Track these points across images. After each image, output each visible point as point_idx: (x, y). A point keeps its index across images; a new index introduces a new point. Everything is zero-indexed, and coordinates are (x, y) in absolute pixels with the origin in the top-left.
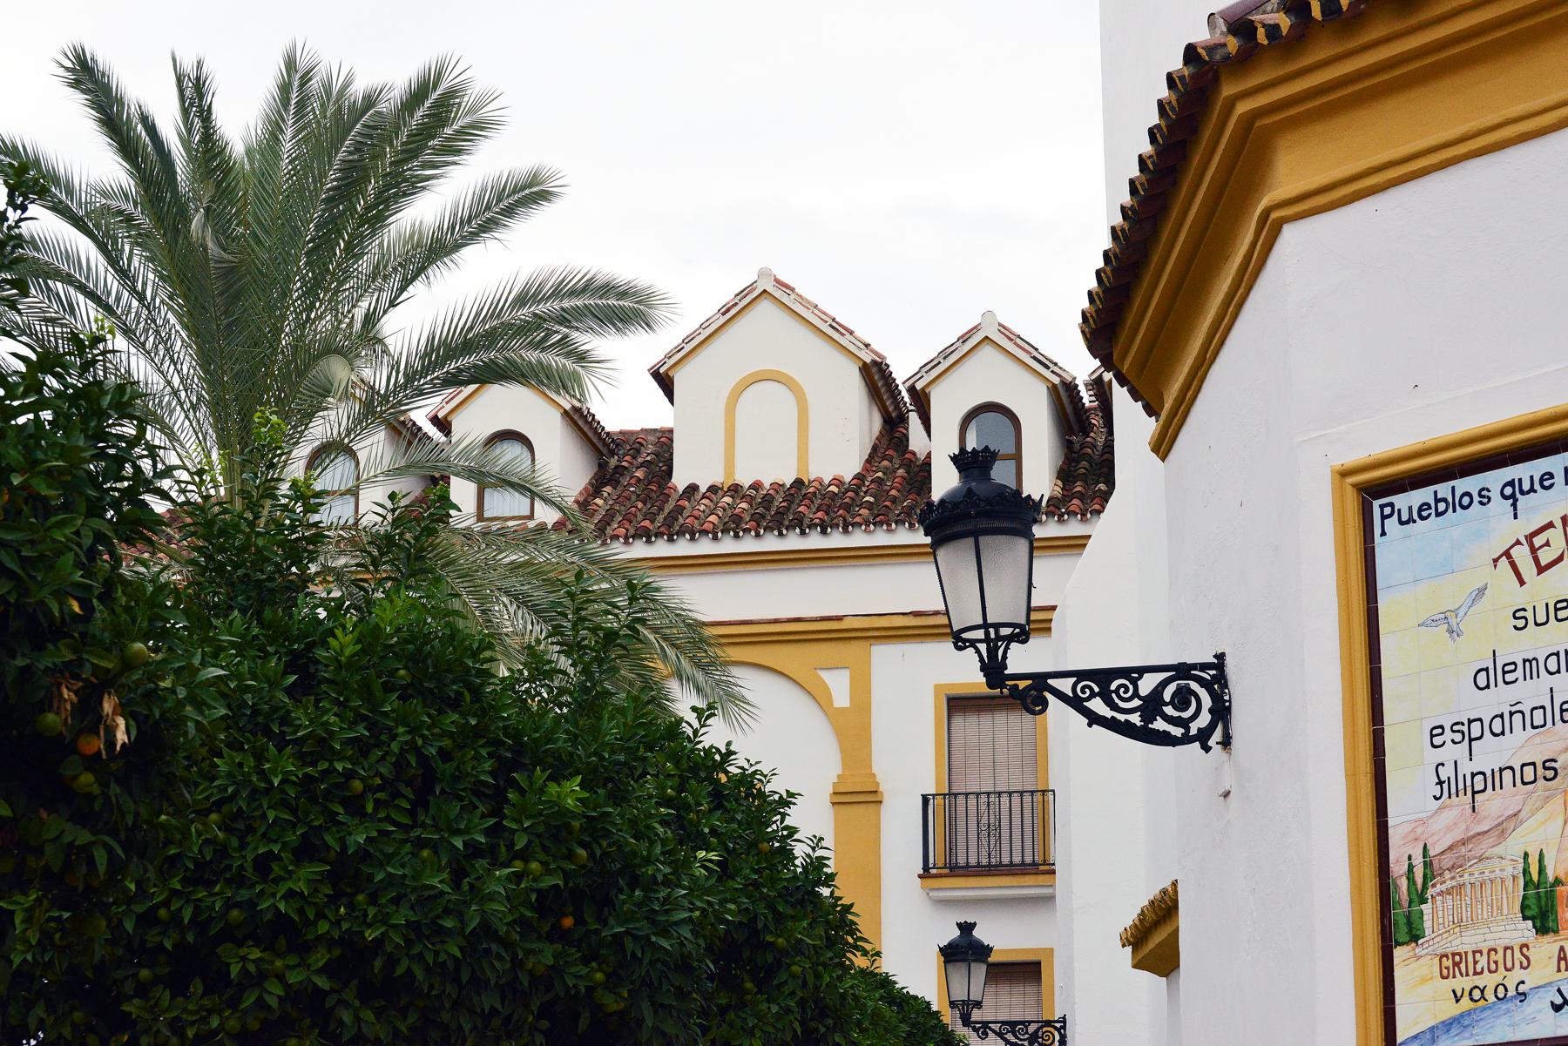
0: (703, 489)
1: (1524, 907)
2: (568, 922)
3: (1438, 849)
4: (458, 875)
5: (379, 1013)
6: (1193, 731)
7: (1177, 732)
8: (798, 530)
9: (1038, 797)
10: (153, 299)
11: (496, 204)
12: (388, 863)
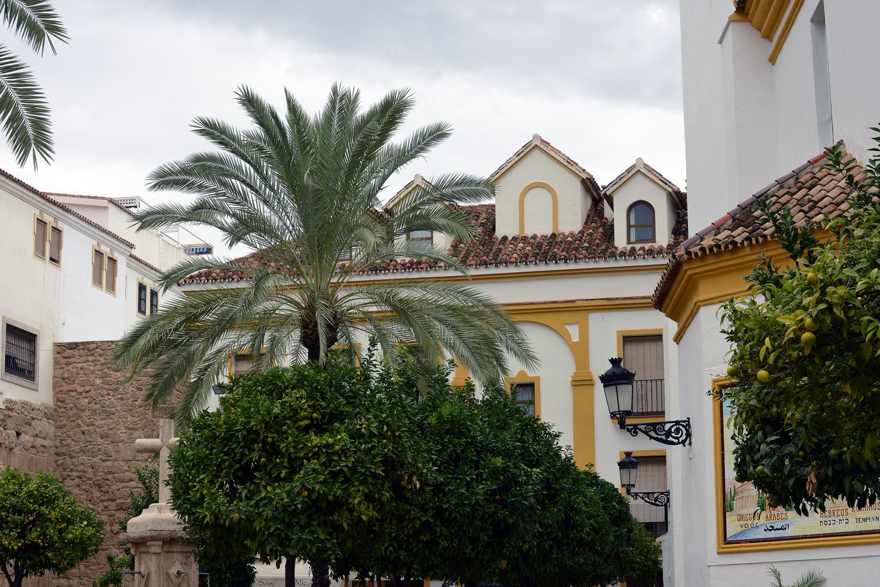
0: (510, 238)
1: (758, 503)
2: (498, 497)
3: (738, 486)
7: (676, 441)
8: (554, 261)
9: (659, 382)
10: (278, 189)
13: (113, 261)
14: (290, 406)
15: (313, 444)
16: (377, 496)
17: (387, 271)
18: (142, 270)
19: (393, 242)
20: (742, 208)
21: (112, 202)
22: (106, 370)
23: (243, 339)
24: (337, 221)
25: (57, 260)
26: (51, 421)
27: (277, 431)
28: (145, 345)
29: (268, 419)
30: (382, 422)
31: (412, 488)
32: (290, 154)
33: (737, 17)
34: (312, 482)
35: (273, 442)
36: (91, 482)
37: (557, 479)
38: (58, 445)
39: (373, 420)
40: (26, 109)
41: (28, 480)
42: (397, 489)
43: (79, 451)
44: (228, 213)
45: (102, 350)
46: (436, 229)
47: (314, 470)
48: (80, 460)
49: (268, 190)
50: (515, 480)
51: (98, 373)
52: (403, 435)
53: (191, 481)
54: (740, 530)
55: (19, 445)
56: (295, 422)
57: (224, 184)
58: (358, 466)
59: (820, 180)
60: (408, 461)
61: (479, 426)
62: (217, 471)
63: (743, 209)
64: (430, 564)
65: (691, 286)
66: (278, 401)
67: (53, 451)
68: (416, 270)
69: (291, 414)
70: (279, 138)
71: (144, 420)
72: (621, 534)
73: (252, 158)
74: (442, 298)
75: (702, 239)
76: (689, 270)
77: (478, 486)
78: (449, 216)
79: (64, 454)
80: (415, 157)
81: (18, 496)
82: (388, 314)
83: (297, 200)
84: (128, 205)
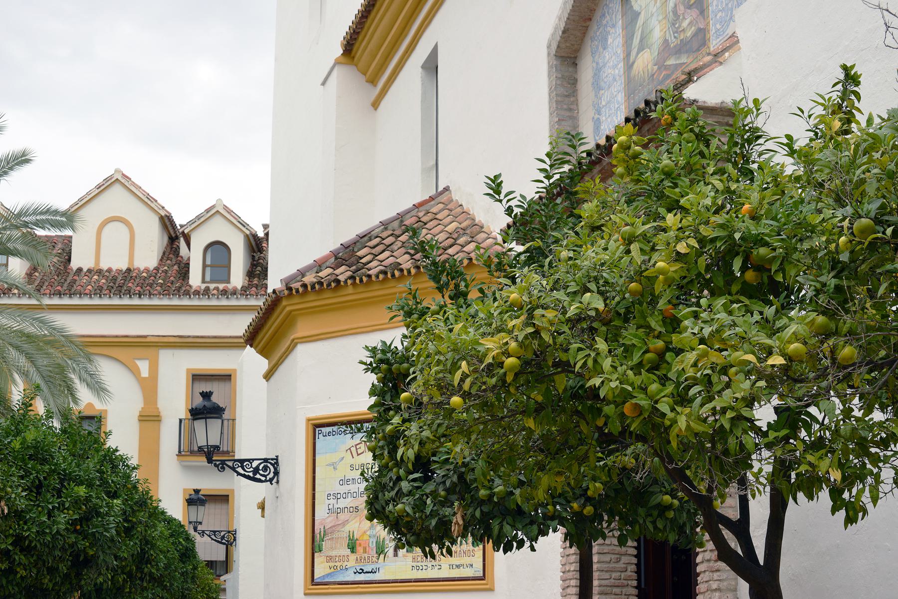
0: (85, 270)
1: (348, 545)
2: (78, 527)
5: (25, 556)
6: (268, 479)
7: (263, 479)
9: (231, 422)
20: (345, 247)
33: (343, 60)
37: (134, 511)
46: (13, 255)
50: (96, 511)
54: (328, 571)
59: (425, 224)
63: (346, 248)
64: (7, 593)
65: (289, 322)
72: (186, 572)
75: (303, 275)
76: (287, 306)
78: (30, 243)
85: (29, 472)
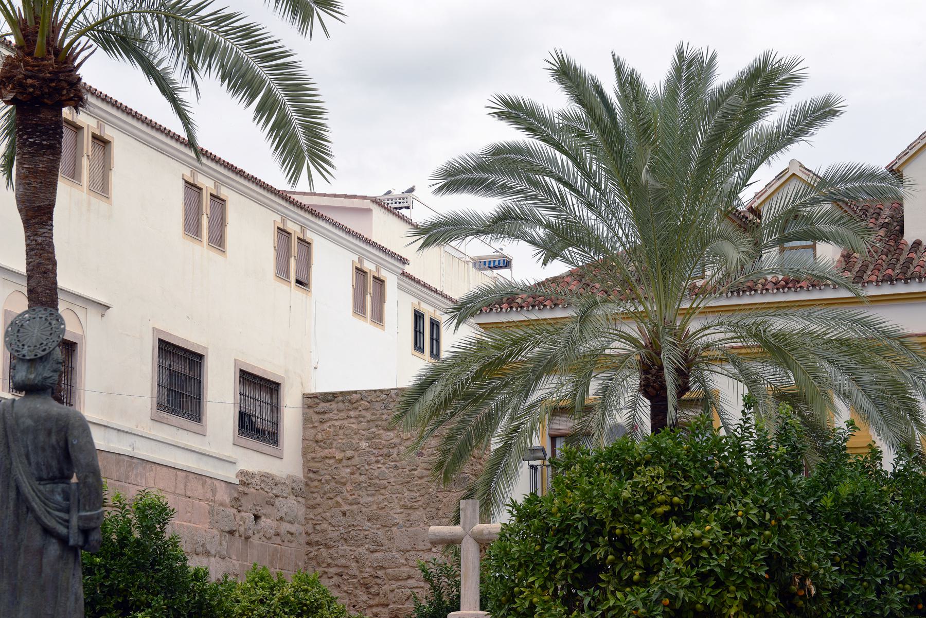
2: (921, 606)
4: (879, 593)
10: (606, 188)
11: (804, 120)
12: (852, 589)
13: (379, 281)
14: (643, 487)
15: (675, 537)
16: (759, 605)
17: (753, 292)
18: (420, 293)
19: (761, 256)
21: (377, 203)
22: (374, 429)
23: (565, 388)
24: (687, 227)
25: (306, 282)
26: (300, 499)
27: (627, 521)
28: (434, 399)
29: (615, 506)
30: (763, 508)
31: (805, 595)
32: (621, 141)
34: (675, 586)
35: (623, 535)
36: (355, 581)
38: (310, 531)
39: (752, 505)
40: (296, 111)
41: (282, 582)
42: (785, 595)
43: (338, 538)
44: (540, 223)
45: (368, 402)
47: (677, 571)
48: (339, 551)
49: (592, 190)
51: (364, 433)
52: (791, 525)
53: (517, 586)
55: (259, 532)
56: (650, 509)
57: (536, 184)
58: (733, 566)
60: (799, 558)
61: (890, 508)
62: (551, 573)
66: (629, 481)
67: (303, 539)
68: (793, 289)
69: (645, 499)
70: (606, 119)
71: (427, 496)
73: (571, 148)
74: (832, 330)
77: (892, 592)
78: (838, 220)
79: (318, 543)
80: (793, 143)
81: (268, 605)
82: (756, 350)
83: (631, 203)
84: (398, 205)
85: (847, 536)
